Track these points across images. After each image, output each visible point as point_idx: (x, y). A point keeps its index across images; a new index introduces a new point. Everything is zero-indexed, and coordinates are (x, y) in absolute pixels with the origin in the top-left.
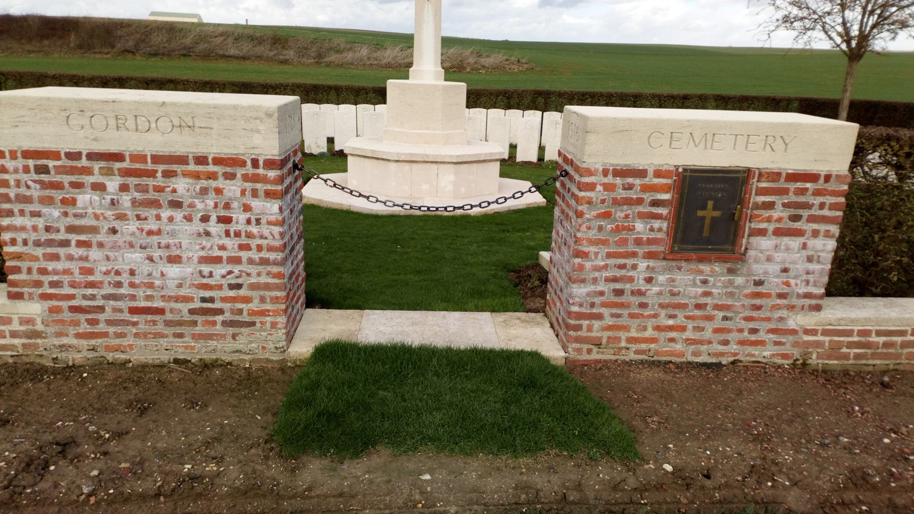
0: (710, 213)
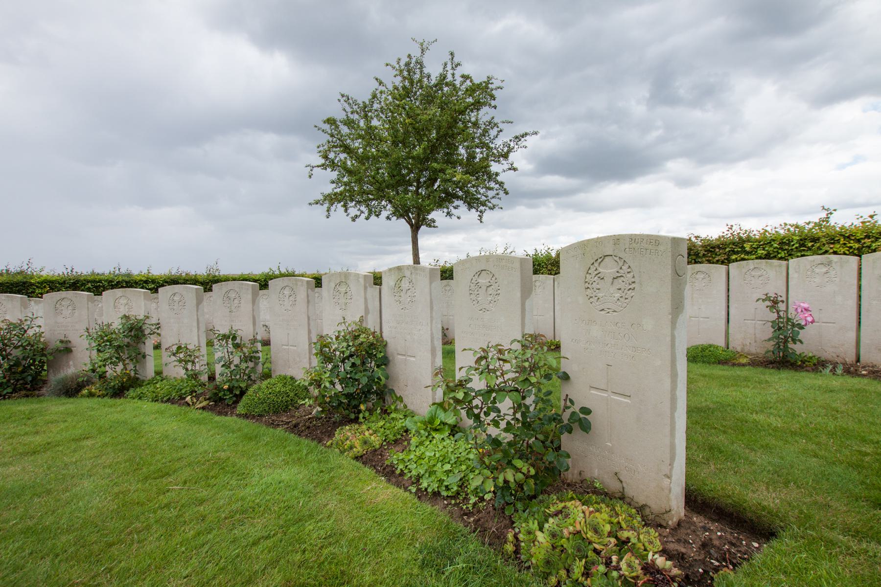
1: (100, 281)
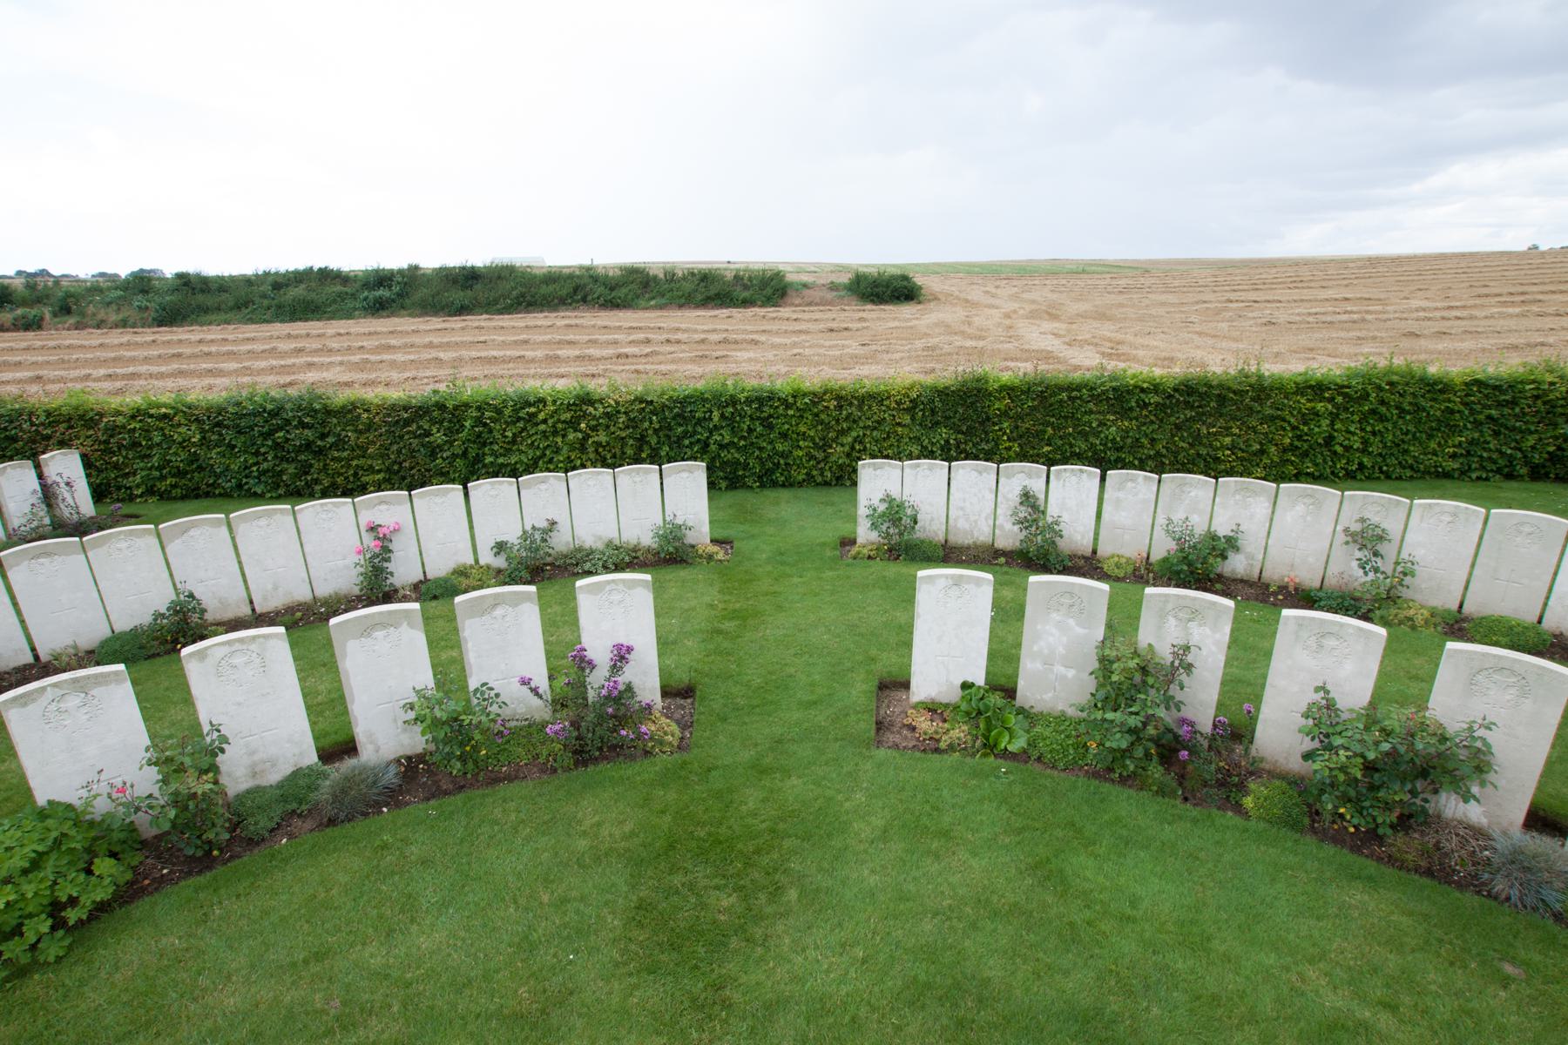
1: (1079, 388)
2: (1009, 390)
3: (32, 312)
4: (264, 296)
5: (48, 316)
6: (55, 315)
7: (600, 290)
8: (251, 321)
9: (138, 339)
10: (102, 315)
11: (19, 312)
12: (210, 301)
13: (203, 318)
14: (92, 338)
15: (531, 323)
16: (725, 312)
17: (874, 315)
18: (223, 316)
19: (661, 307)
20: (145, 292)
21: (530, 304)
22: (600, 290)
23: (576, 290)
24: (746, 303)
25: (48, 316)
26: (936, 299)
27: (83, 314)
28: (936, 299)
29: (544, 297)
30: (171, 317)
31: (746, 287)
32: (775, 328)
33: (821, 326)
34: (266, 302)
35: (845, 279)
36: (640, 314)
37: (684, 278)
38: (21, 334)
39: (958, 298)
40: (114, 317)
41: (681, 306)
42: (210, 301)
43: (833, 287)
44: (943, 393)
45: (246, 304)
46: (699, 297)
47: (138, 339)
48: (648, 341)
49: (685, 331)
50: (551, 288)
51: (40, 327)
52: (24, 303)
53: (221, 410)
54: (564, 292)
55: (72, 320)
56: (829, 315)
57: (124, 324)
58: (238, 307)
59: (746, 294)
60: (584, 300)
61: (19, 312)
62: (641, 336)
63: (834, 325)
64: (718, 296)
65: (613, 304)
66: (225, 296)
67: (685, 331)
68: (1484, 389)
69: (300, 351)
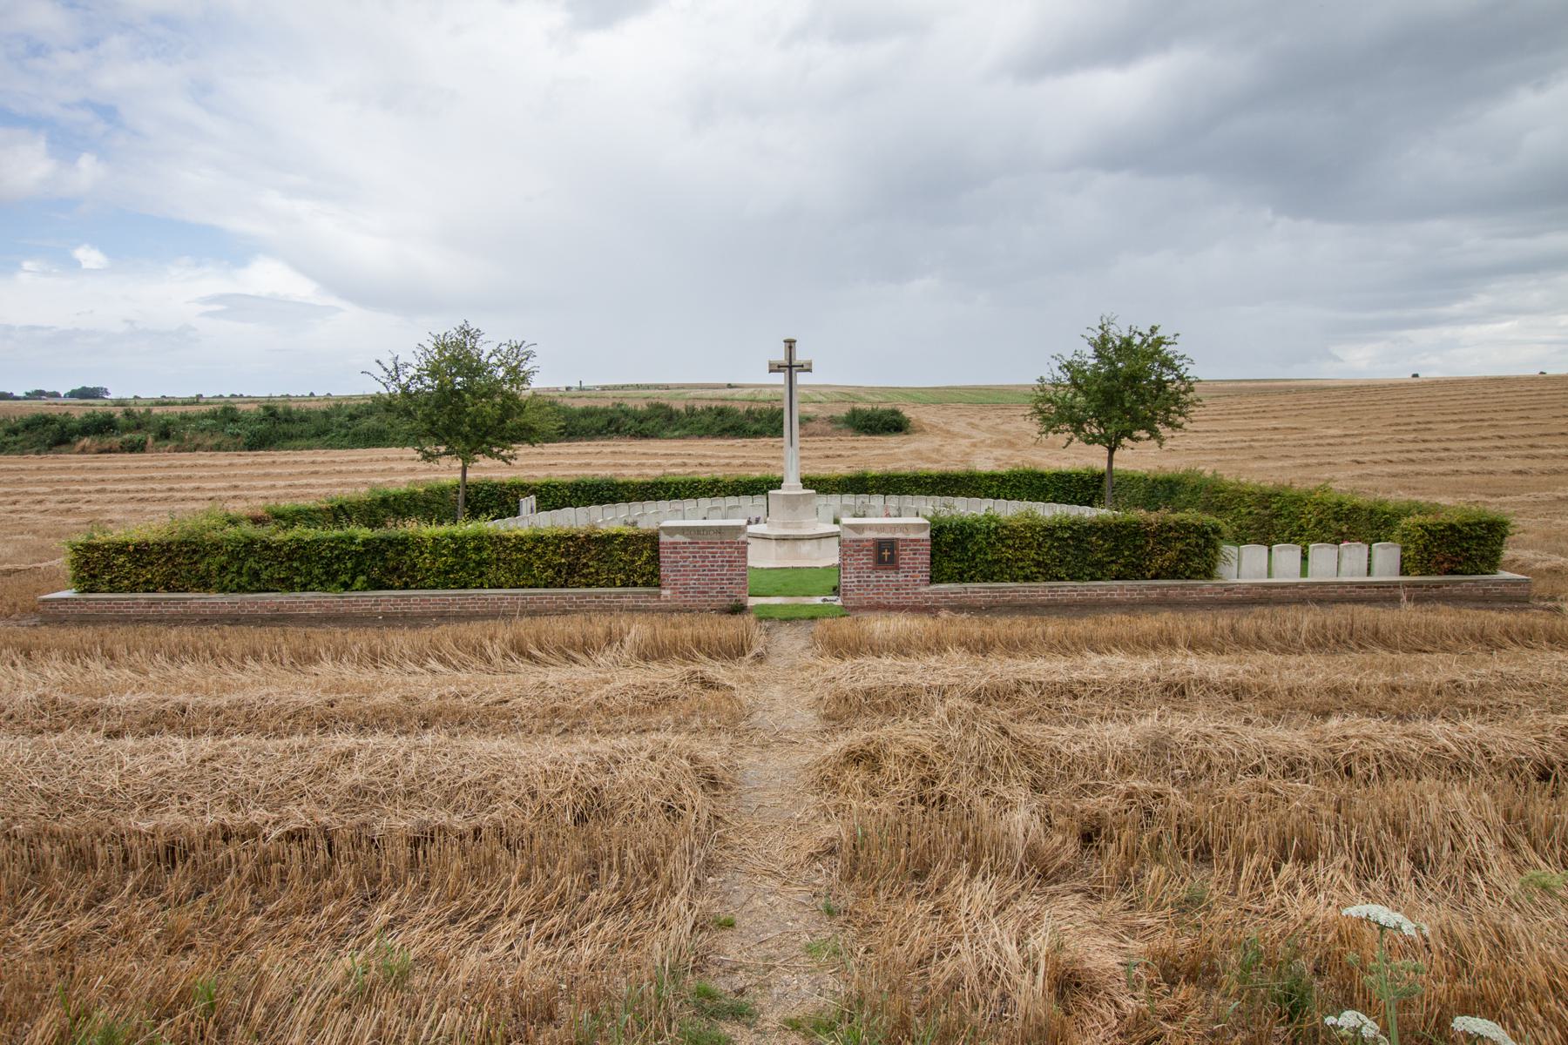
0: (886, 553)
2: (875, 478)
3: (137, 436)
4: (341, 425)
5: (150, 440)
6: (156, 439)
7: (631, 423)
8: (332, 447)
9: (259, 460)
10: (198, 440)
11: (127, 436)
12: (295, 429)
13: (287, 444)
14: (186, 458)
15: (298, 459)
16: (739, 442)
17: (864, 444)
18: (304, 442)
19: (683, 437)
20: (234, 420)
21: (571, 434)
22: (631, 423)
23: (610, 422)
24: (757, 434)
25: (150, 440)
26: (922, 431)
27: (182, 440)
28: (922, 431)
29: (583, 429)
30: (259, 442)
31: (757, 421)
32: (1104, 631)
33: (820, 453)
34: (343, 431)
35: (842, 411)
36: (668, 443)
37: (703, 413)
38: (127, 456)
39: (941, 429)
40: (210, 442)
41: (700, 437)
42: (295, 429)
43: (832, 420)
44: (850, 479)
45: (325, 433)
46: (717, 429)
47: (259, 460)
48: (685, 465)
49: (711, 457)
50: (589, 421)
51: (143, 450)
52: (128, 429)
53: (578, 485)
54: (600, 424)
55: (172, 445)
56: (829, 445)
57: (218, 448)
58: (318, 435)
59: (757, 427)
60: (617, 431)
61: (127, 436)
62: (679, 461)
63: (830, 453)
64: (732, 428)
65: (643, 435)
66: (305, 426)
67: (711, 457)
68: (1059, 476)
69: (266, 475)
